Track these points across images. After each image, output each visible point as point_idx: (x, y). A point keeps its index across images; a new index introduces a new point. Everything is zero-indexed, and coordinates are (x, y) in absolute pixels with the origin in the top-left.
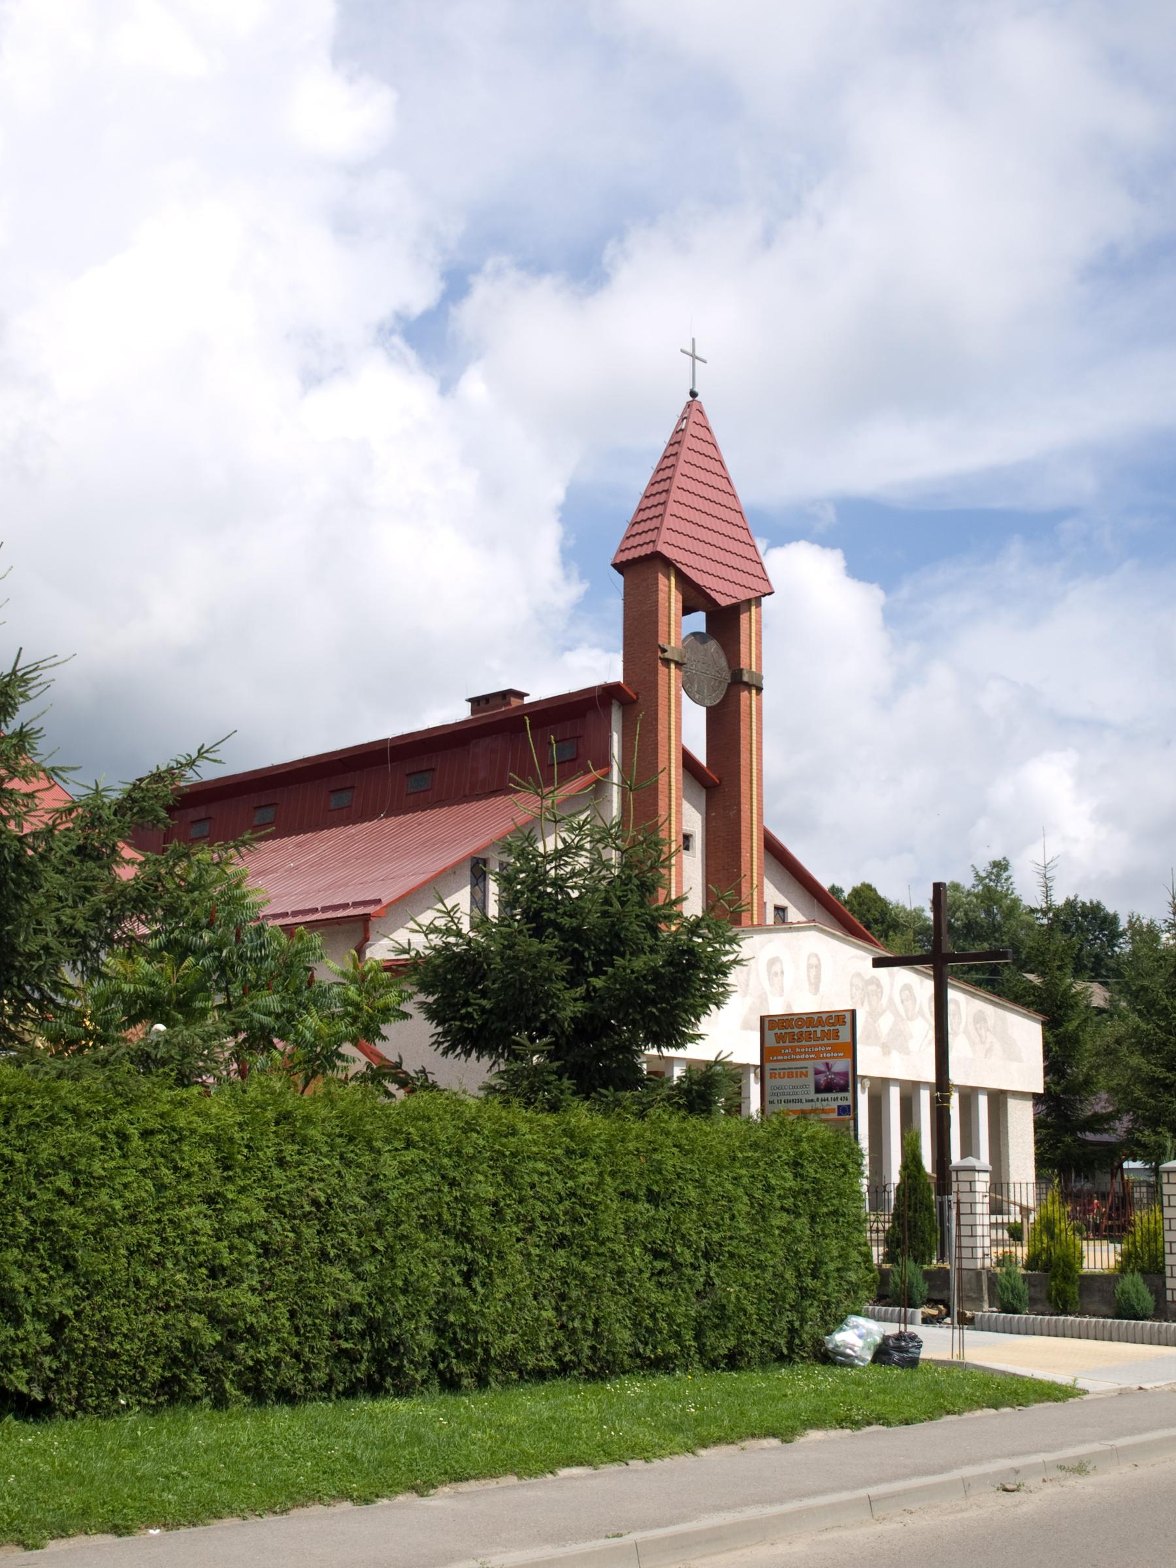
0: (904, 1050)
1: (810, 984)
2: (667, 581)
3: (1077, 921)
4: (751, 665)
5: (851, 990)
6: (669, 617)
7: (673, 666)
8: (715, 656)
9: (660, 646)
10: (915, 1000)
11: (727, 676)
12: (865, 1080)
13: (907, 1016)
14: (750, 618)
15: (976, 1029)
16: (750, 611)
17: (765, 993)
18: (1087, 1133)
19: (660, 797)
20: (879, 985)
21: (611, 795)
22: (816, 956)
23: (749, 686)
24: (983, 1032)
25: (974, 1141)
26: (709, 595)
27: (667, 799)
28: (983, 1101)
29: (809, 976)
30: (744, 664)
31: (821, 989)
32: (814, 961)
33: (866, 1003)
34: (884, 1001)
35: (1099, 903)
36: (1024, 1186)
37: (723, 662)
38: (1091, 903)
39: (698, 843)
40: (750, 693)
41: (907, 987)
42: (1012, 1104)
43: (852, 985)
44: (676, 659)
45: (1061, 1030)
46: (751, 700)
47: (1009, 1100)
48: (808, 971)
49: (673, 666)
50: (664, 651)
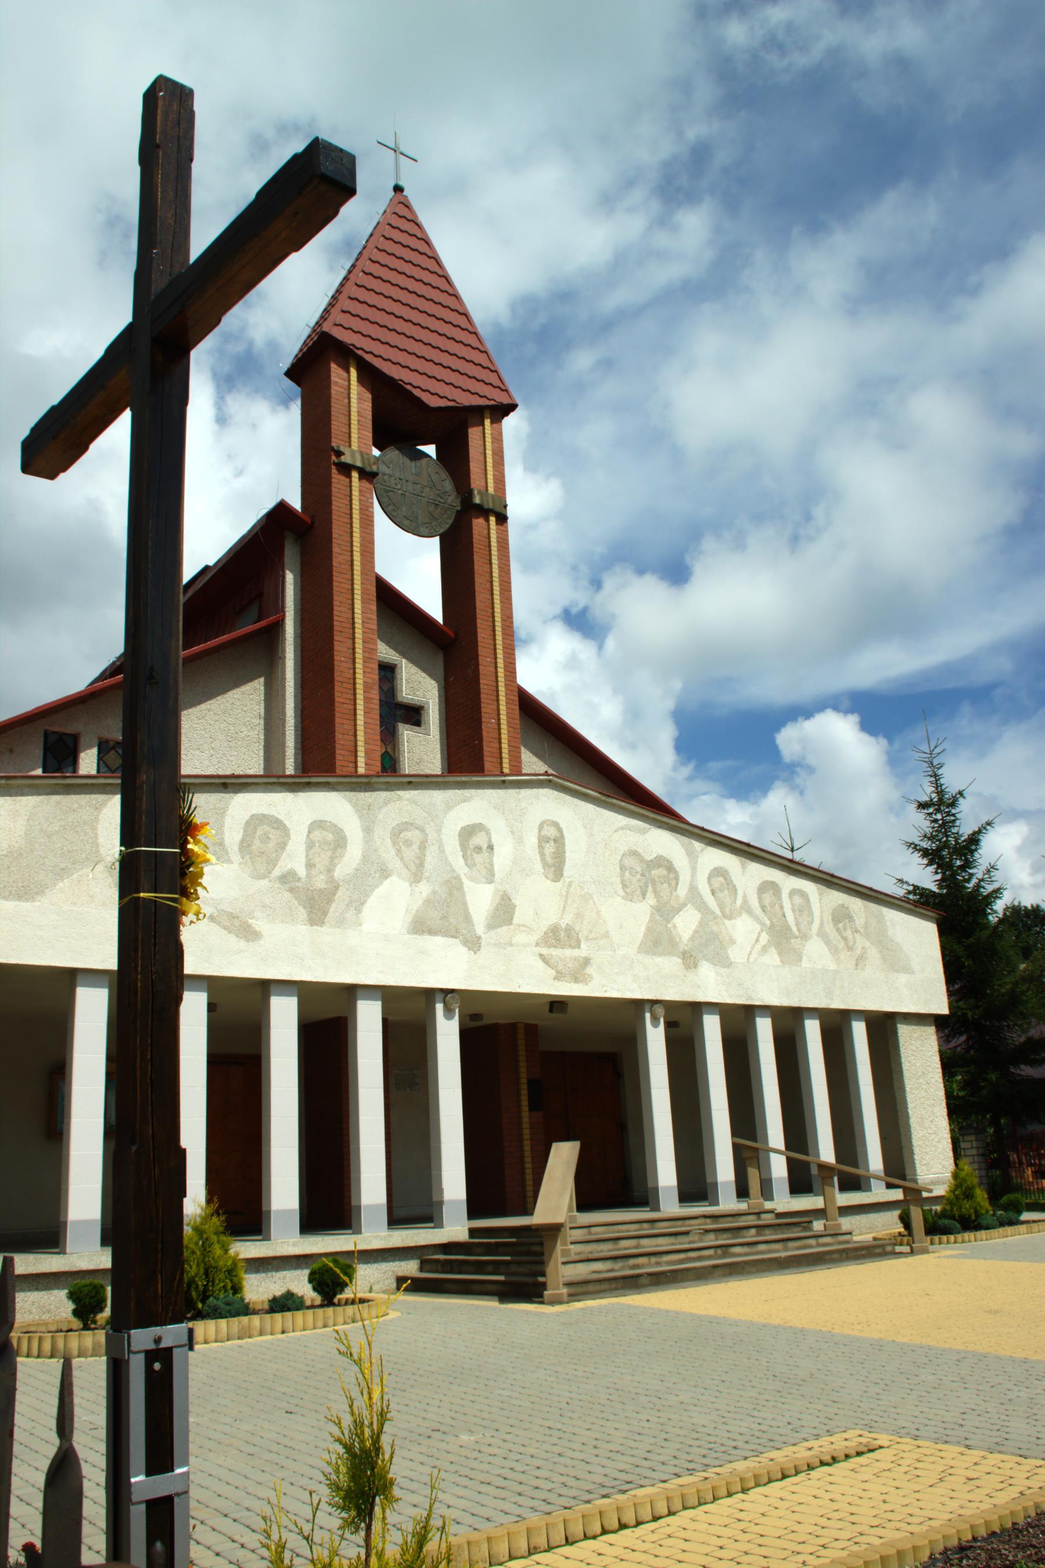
0: (721, 960)
1: (545, 864)
2: (345, 375)
3: (1022, 921)
4: (487, 487)
5: (622, 876)
6: (349, 416)
7: (355, 475)
8: (435, 477)
9: (333, 449)
10: (734, 890)
11: (453, 500)
12: (656, 1007)
13: (723, 912)
14: (484, 433)
15: (838, 930)
16: (483, 425)
17: (458, 878)
18: (1023, 1067)
19: (337, 637)
20: (670, 868)
21: (284, 651)
22: (556, 825)
23: (484, 512)
24: (848, 933)
25: (851, 1087)
26: (418, 401)
27: (350, 642)
28: (859, 1031)
29: (542, 854)
30: (476, 482)
31: (565, 874)
32: (551, 832)
33: (650, 894)
34: (682, 891)
35: (1038, 906)
36: (35, 1351)
37: (448, 485)
38: (1032, 906)
39: (433, 715)
40: (487, 521)
41: (719, 872)
42: (904, 1031)
43: (623, 868)
44: (359, 464)
45: (972, 940)
46: (489, 529)
47: (899, 1026)
48: (540, 846)
49: (355, 475)
50: (339, 454)
